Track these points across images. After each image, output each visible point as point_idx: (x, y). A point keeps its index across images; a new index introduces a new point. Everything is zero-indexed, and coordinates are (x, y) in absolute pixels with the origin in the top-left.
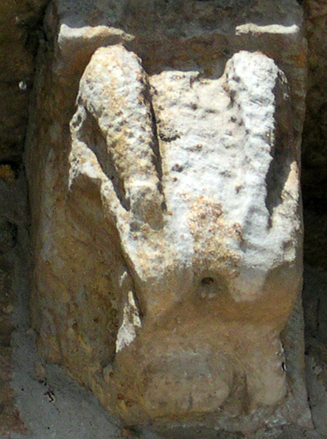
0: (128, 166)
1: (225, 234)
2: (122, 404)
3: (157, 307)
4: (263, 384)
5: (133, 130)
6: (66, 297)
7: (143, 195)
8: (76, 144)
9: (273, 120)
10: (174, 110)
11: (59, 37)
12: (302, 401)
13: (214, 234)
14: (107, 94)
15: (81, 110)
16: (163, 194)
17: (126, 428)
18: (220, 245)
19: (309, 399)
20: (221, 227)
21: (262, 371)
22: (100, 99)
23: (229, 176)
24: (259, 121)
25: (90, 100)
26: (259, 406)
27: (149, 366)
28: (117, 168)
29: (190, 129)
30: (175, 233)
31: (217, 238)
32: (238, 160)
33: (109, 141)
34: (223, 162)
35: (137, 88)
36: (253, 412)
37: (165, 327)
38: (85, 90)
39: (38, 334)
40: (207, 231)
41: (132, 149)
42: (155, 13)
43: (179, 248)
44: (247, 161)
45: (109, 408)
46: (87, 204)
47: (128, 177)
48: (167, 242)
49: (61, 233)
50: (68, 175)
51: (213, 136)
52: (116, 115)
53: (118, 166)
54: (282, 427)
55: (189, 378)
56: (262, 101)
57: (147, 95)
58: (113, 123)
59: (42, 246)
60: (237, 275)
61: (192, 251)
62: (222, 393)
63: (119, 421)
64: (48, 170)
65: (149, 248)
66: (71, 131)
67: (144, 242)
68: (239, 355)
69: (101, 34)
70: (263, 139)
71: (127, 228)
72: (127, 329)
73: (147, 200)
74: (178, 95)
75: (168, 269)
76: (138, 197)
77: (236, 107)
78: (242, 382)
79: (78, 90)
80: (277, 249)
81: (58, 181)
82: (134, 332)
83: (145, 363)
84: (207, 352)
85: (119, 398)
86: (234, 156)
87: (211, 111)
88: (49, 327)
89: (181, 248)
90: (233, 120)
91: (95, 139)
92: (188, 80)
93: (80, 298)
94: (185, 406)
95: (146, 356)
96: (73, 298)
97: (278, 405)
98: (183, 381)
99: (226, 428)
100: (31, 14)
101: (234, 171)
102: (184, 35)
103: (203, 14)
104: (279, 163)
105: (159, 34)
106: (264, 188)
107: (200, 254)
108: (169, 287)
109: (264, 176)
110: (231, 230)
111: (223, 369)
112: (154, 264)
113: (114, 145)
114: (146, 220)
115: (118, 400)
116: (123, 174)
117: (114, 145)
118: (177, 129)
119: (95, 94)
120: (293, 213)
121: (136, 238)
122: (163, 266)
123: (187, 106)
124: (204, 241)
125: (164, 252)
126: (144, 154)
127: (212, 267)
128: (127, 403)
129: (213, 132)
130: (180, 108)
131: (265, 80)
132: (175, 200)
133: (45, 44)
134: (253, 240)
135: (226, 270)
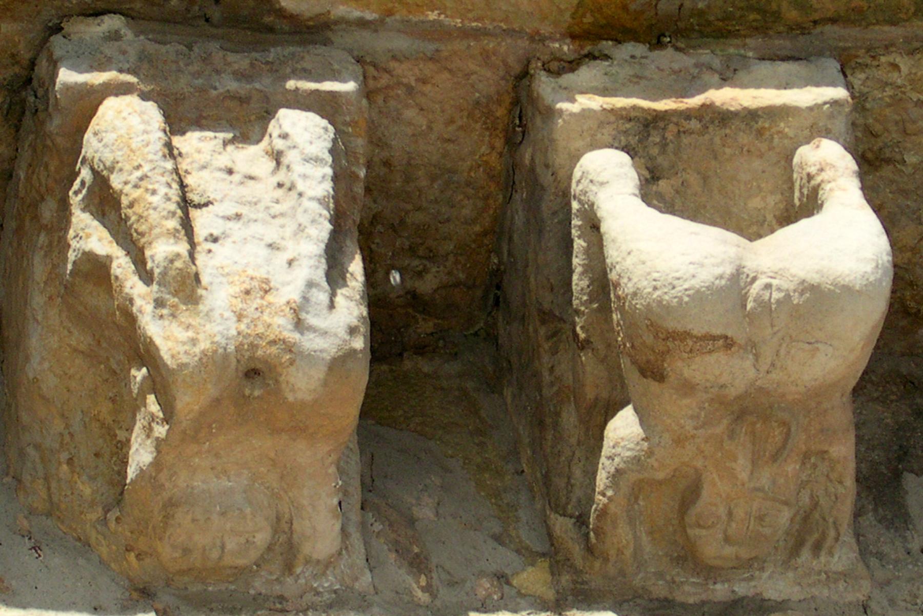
0: (151, 229)
1: (276, 313)
2: (132, 557)
3: (188, 404)
4: (314, 528)
5: (156, 186)
6: (58, 426)
7: (172, 261)
8: (78, 216)
9: (331, 184)
10: (205, 174)
11: (57, 83)
12: (360, 561)
13: (262, 312)
14: (122, 145)
15: (85, 174)
16: (195, 264)
17: (136, 590)
18: (269, 326)
19: (367, 560)
20: (270, 304)
21: (314, 507)
22: (112, 151)
23: (278, 249)
24: (314, 183)
25: (97, 156)
26: (308, 561)
27: (170, 499)
28: (135, 235)
29: (225, 196)
30: (212, 310)
31: (266, 317)
32: (288, 231)
33: (125, 201)
34: (271, 233)
35: (160, 138)
36: (298, 570)
37: (195, 439)
38: (91, 145)
39: (19, 481)
40: (252, 309)
41: (155, 209)
42: (176, 62)
43: (217, 329)
44: (301, 228)
45: (113, 565)
46: (91, 293)
47: (150, 243)
48: (202, 322)
49: (54, 342)
50: (66, 259)
51: (256, 204)
52: (134, 168)
53: (136, 231)
54: (335, 592)
55: (223, 514)
56: (317, 160)
57: (171, 152)
58: (129, 178)
59: (27, 358)
60: (292, 362)
61: (234, 332)
62: (262, 538)
63: (127, 581)
64: (37, 259)
65: (180, 329)
66: (71, 202)
67: (171, 322)
68: (286, 487)
69: (111, 80)
70: (321, 204)
71: (149, 308)
72: (143, 448)
73: (177, 269)
74: (209, 157)
75: (204, 353)
76: (165, 264)
77: (283, 170)
78: (287, 530)
79: (81, 148)
80: (343, 334)
81: (50, 273)
82: (153, 449)
83: (166, 495)
84: (246, 482)
85: (127, 550)
86: (282, 226)
87: (251, 178)
88: (35, 468)
89: (220, 328)
90: (280, 185)
91: (103, 211)
92: (221, 142)
93: (77, 427)
94: (215, 554)
95: (167, 485)
96: (67, 426)
97: (331, 562)
98: (215, 517)
99: (264, 591)
100: (17, 69)
101: (283, 243)
102: (215, 89)
103: (236, 67)
104: (337, 242)
105: (183, 84)
106: (323, 261)
107: (244, 337)
108: (205, 376)
109: (323, 246)
110: (284, 307)
111: (266, 503)
112: (186, 347)
113: (131, 206)
114: (175, 294)
115: (127, 553)
116: (143, 240)
117: (131, 206)
118: (209, 194)
119: (106, 146)
120: (358, 297)
121: (161, 317)
122: (197, 350)
123: (220, 170)
124: (249, 321)
125: (198, 333)
126: (171, 215)
127: (260, 353)
128: (138, 556)
129: (255, 200)
130: (212, 172)
131: (319, 138)
132: (211, 274)
133: (35, 102)
134: (311, 320)
135: (278, 357)
